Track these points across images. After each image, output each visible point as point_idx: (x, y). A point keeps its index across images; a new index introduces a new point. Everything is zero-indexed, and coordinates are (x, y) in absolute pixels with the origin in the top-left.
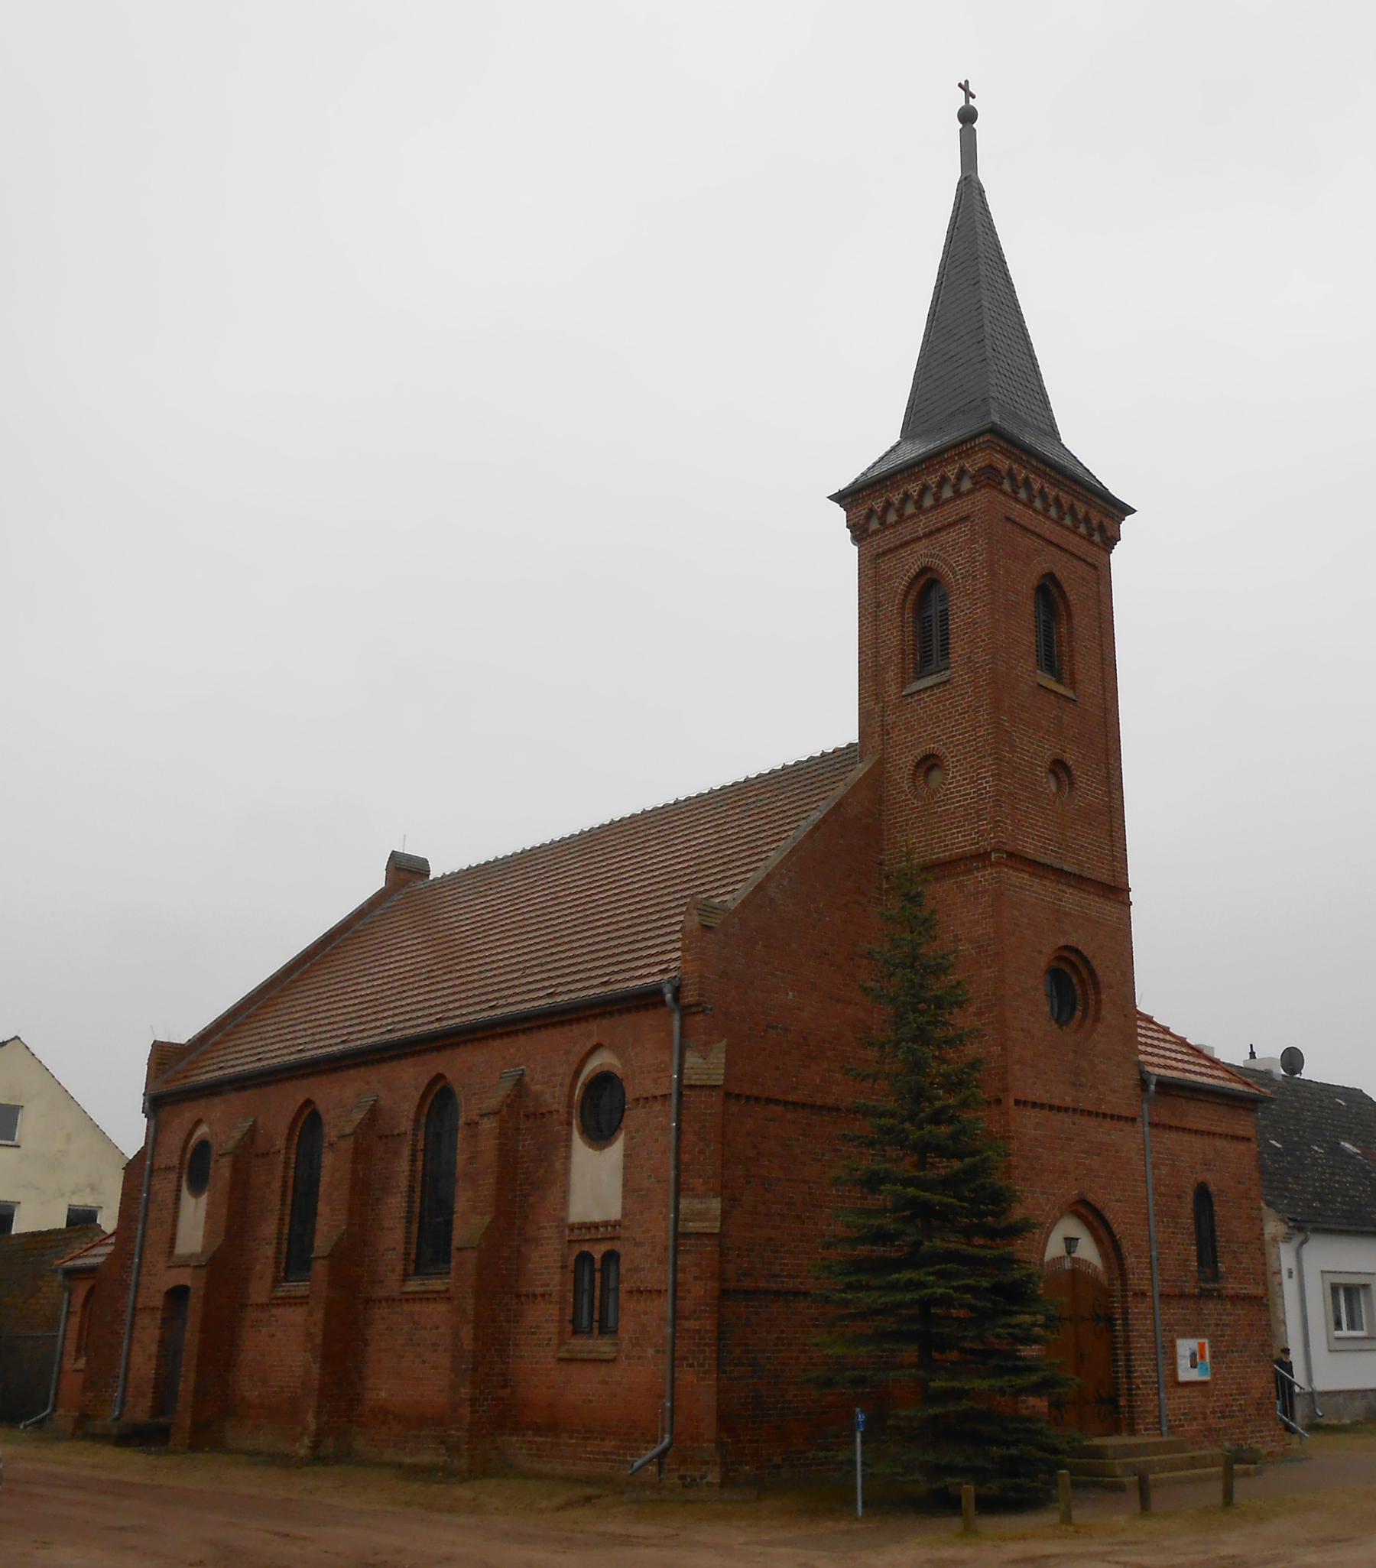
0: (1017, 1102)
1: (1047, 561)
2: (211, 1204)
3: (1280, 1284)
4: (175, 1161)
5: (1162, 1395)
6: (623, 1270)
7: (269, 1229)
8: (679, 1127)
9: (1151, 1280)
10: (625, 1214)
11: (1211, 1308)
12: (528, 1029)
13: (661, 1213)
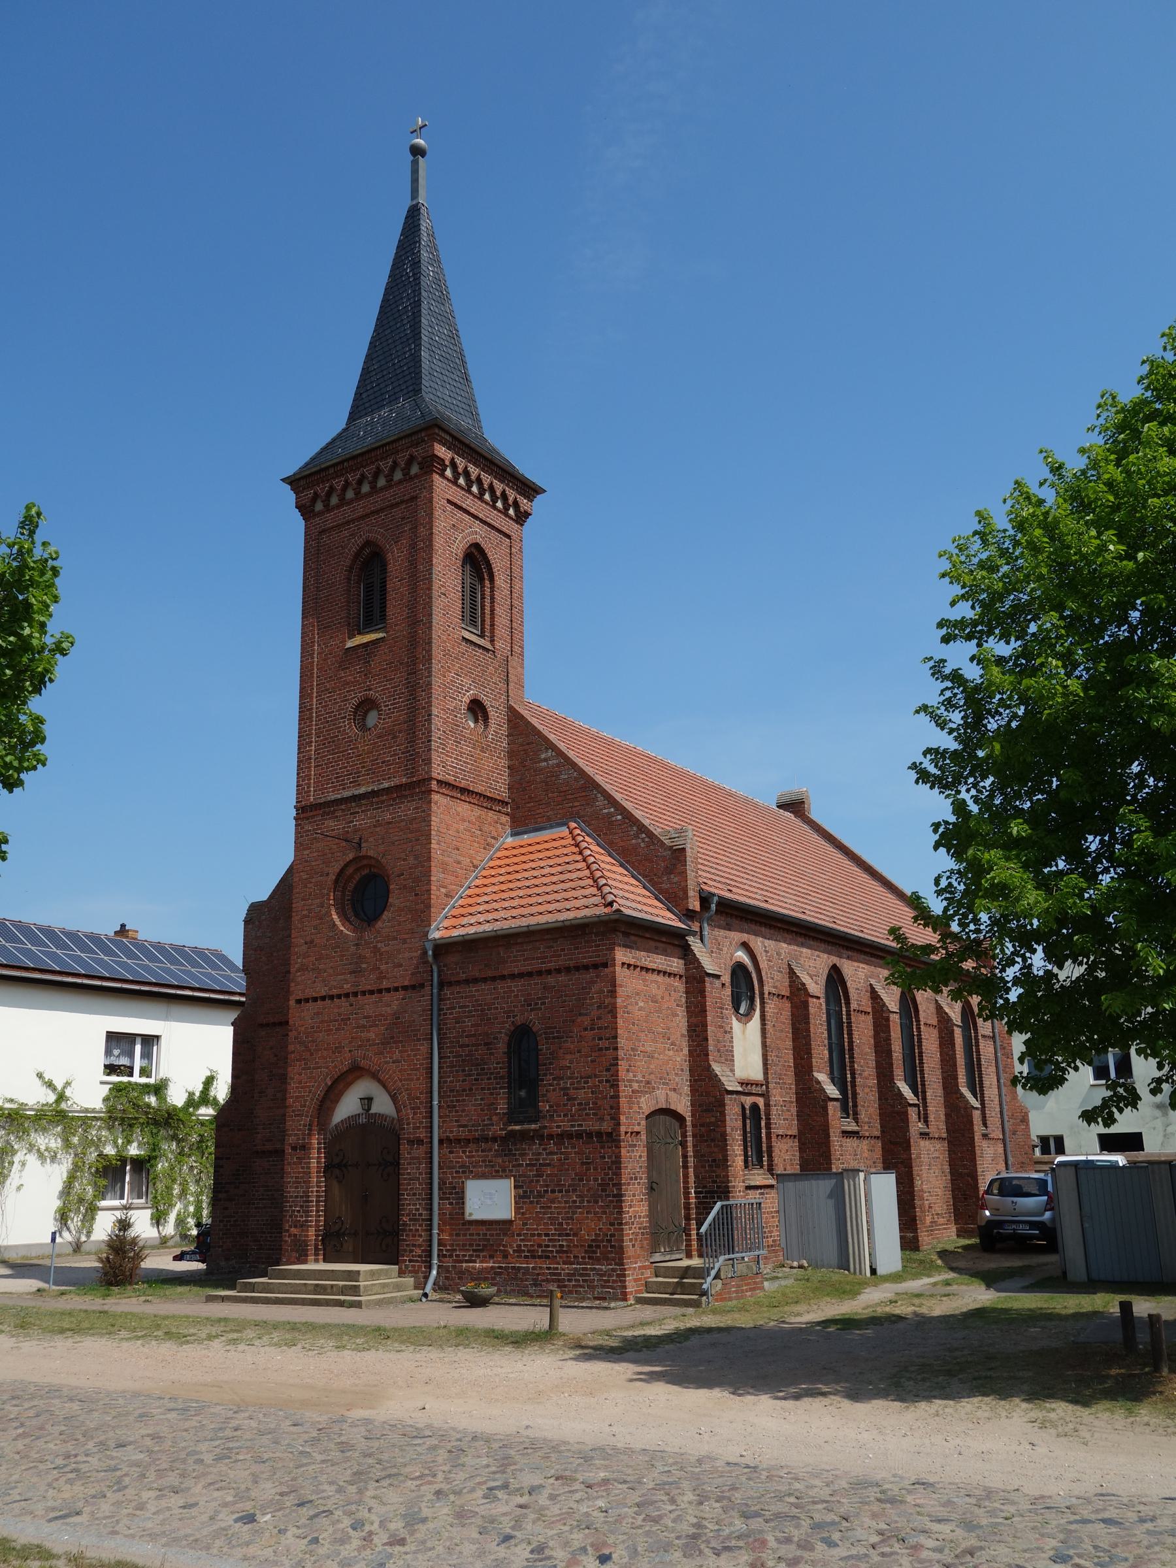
1: (478, 533)
12: (792, 932)
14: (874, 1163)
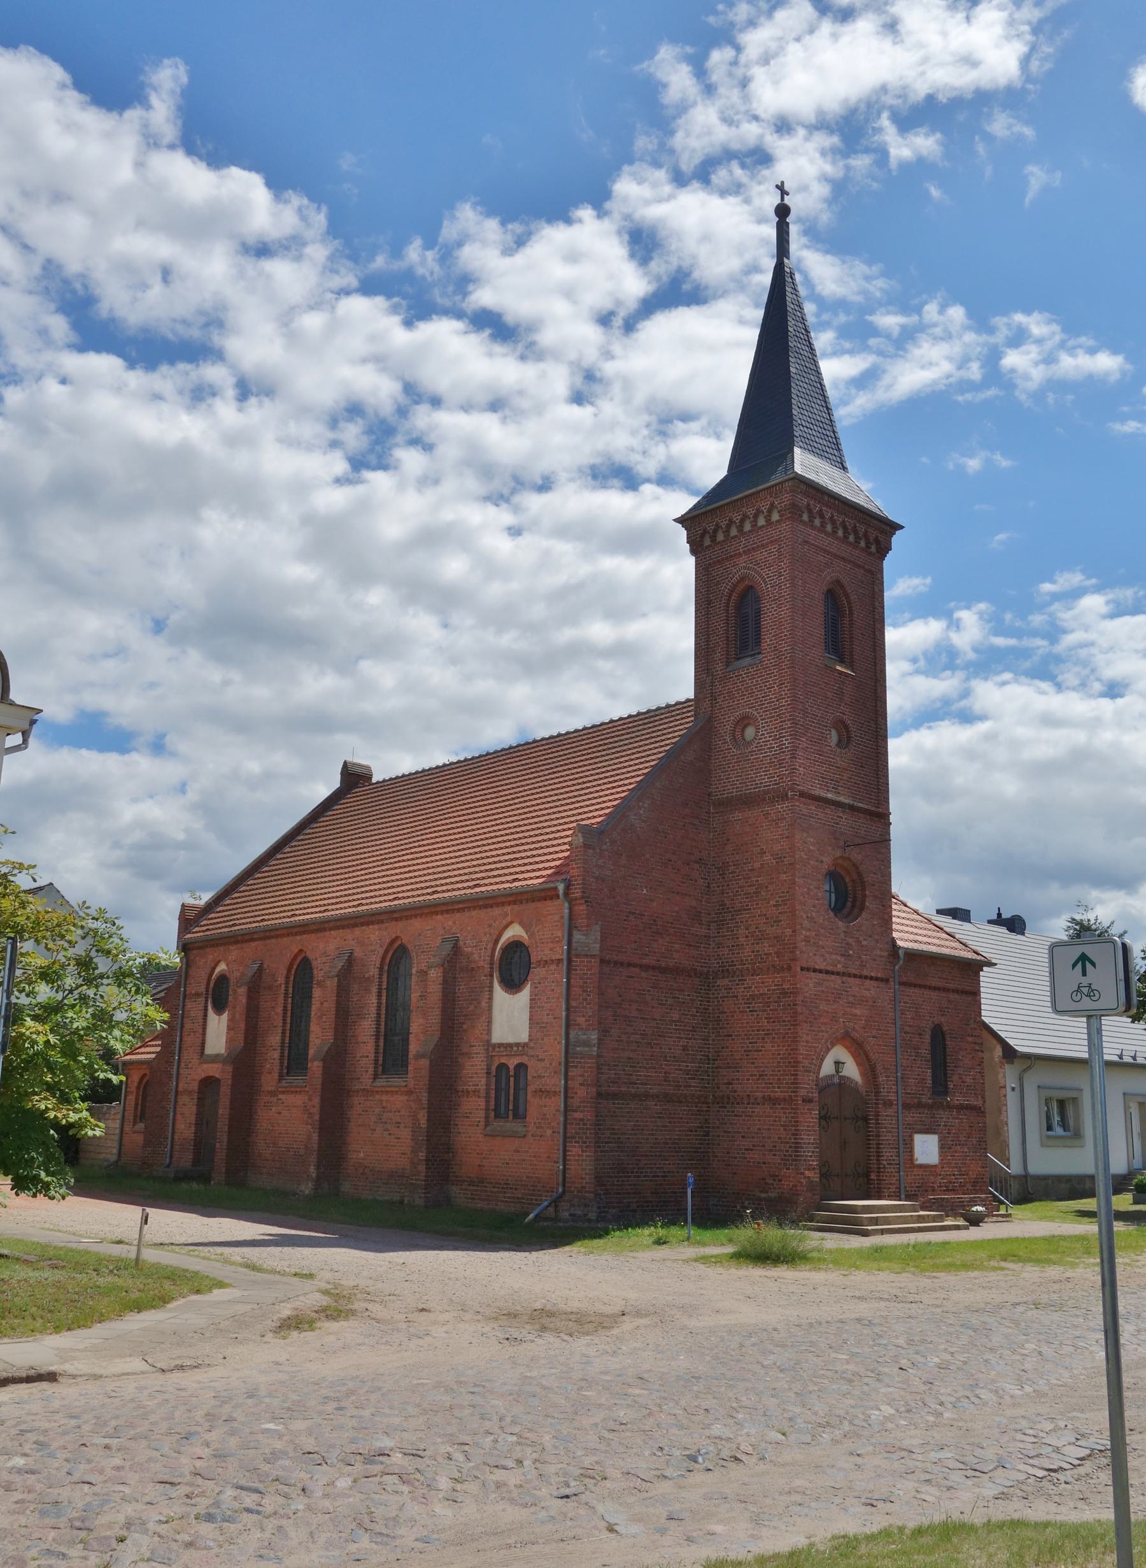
0: (802, 969)
2: (231, 1020)
3: (1005, 1096)
4: (202, 989)
5: (902, 1173)
6: (529, 1078)
7: (275, 1039)
8: (568, 982)
9: (897, 1093)
10: (530, 1040)
11: (943, 1116)
13: (555, 1039)
14: (718, 1088)
